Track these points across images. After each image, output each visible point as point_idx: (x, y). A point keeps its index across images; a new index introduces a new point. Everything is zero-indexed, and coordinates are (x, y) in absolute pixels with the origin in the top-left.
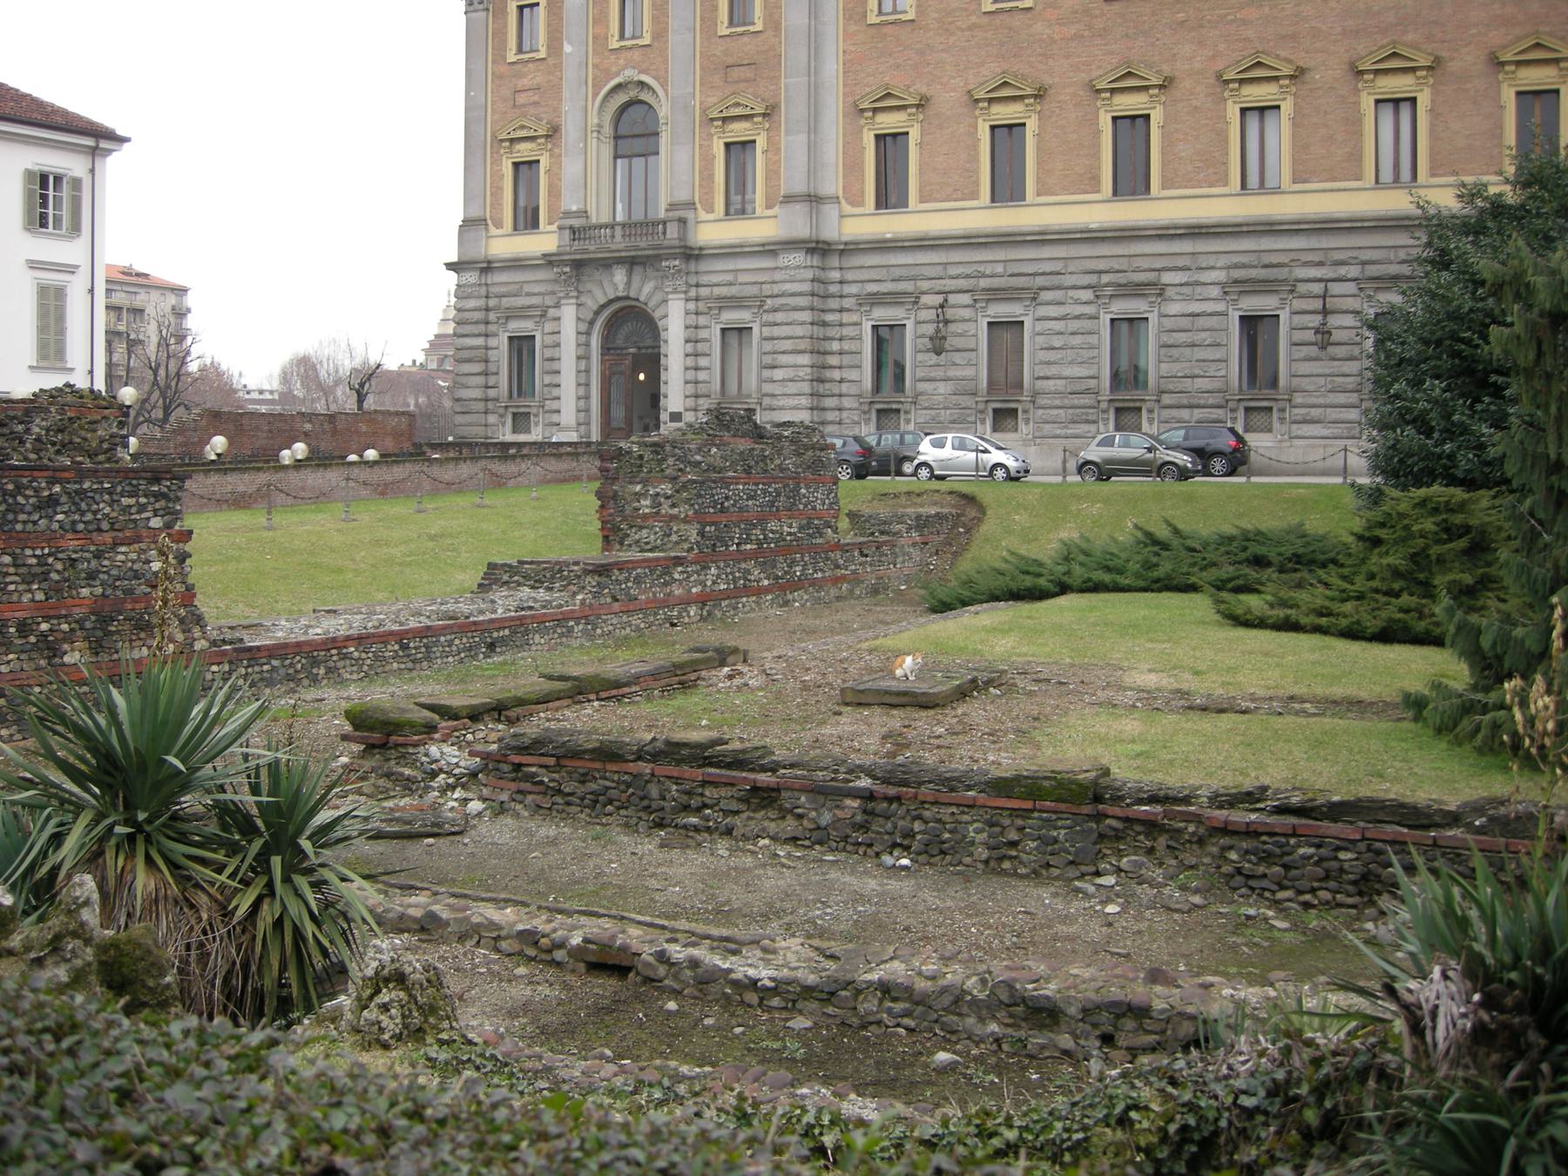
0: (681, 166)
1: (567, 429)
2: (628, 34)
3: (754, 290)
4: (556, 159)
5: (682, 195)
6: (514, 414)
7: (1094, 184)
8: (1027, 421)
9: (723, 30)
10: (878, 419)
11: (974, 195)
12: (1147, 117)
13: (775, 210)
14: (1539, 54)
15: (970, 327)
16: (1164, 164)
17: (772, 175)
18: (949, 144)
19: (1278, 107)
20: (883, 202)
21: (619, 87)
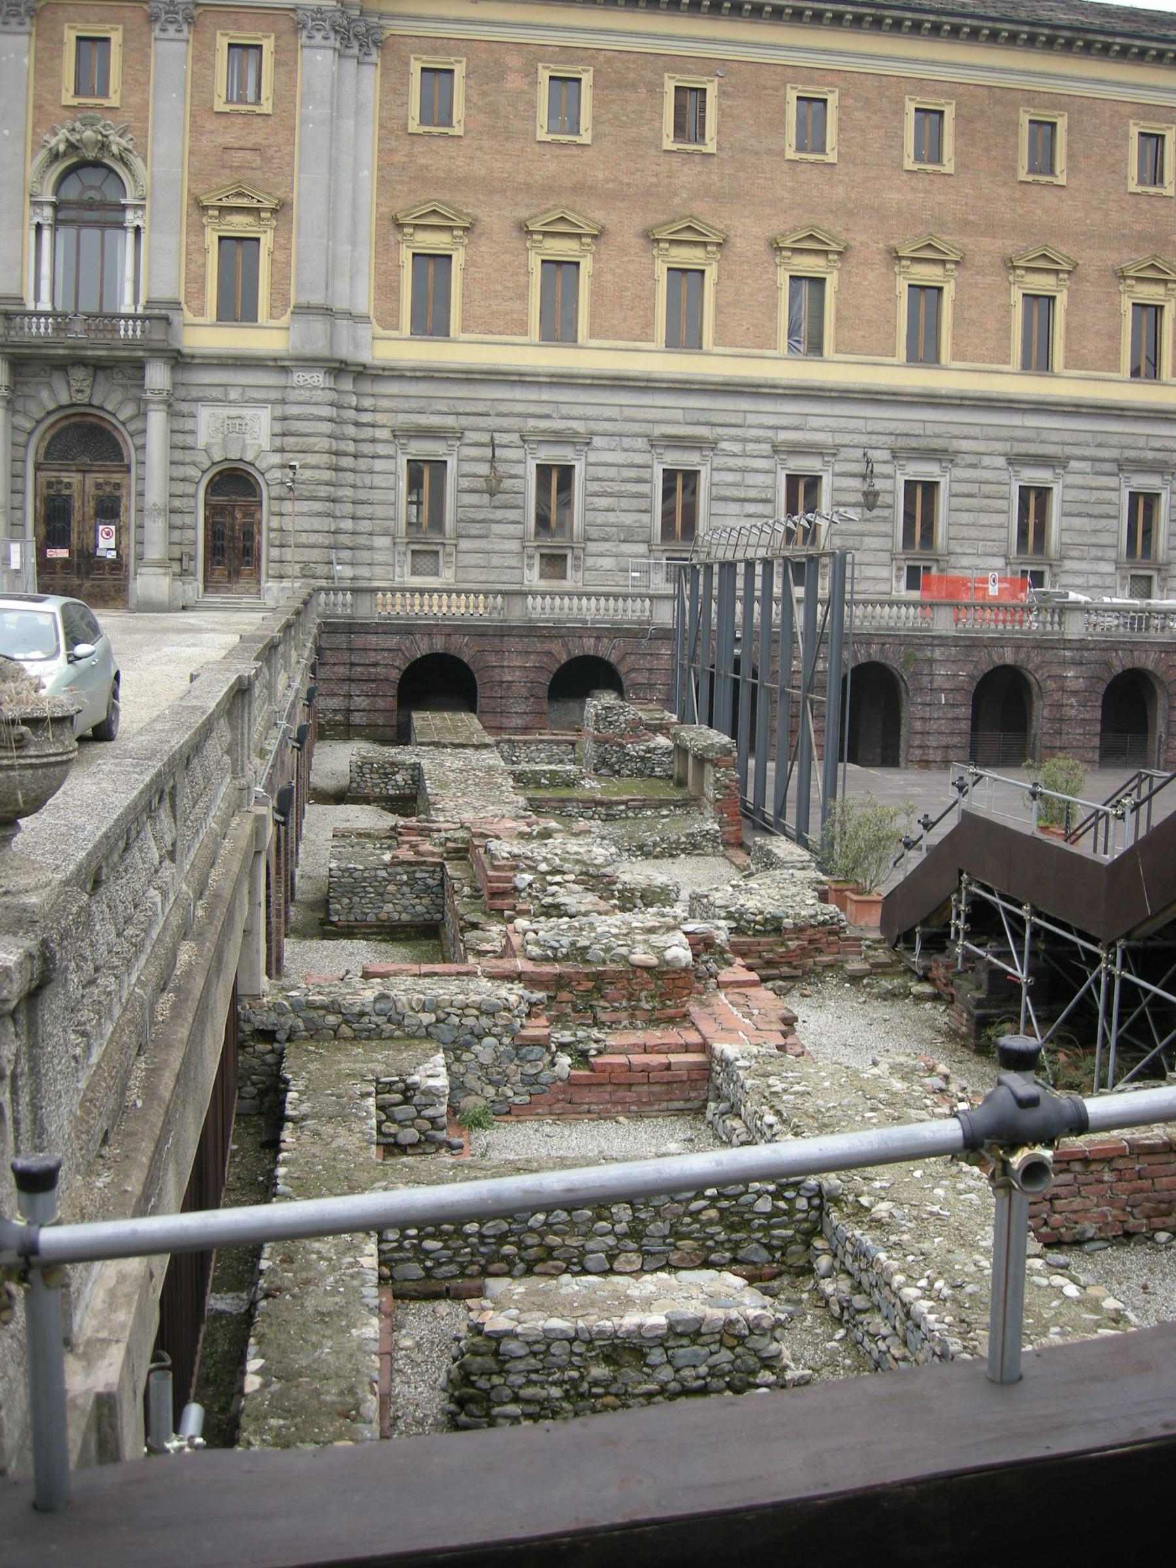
8: (576, 568)
13: (284, 320)
14: (1156, 275)
19: (258, 240)
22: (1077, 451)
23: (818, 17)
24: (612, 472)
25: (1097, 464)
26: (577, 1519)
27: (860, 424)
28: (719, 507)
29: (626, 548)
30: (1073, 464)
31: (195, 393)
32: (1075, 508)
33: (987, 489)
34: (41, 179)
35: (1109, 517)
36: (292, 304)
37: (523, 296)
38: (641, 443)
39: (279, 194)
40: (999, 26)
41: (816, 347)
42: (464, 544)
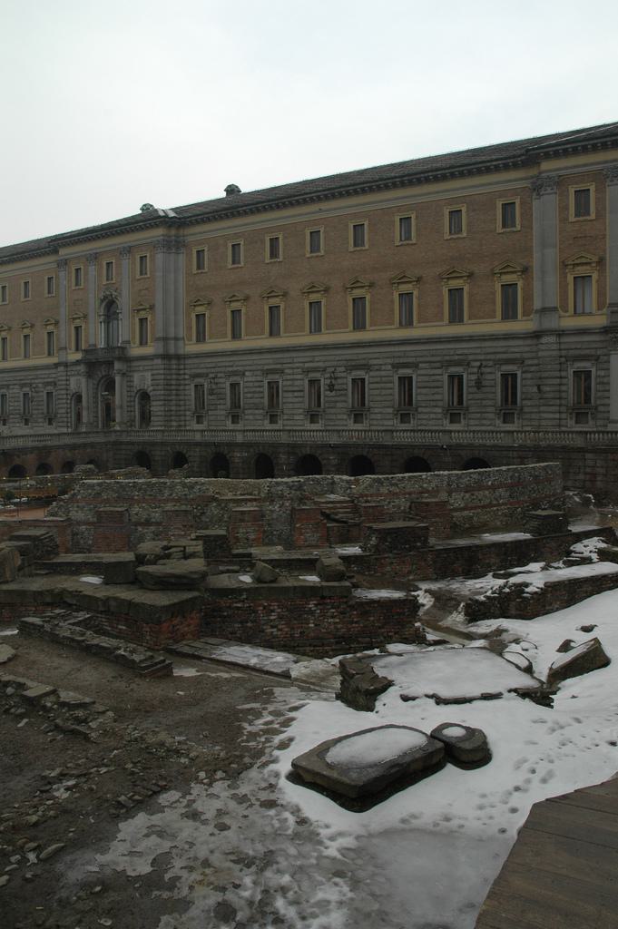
0: (126, 329)
2: (403, 239)
5: (126, 338)
7: (224, 336)
8: (593, 419)
9: (572, 218)
10: (576, 417)
11: (442, 320)
12: (204, 314)
15: (492, 377)
19: (591, 276)
20: (198, 340)
22: (421, 359)
24: (251, 384)
25: (432, 364)
26: (486, 880)
27: (332, 358)
28: (286, 395)
29: (257, 412)
34: (99, 308)
35: (438, 387)
40: (566, 146)
42: (210, 413)
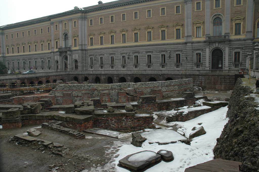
0: (70, 42)
1: (207, 67)
3: (181, 49)
4: (244, 22)
5: (70, 45)
6: (162, 65)
7: (120, 42)
8: (201, 66)
9: (214, 8)
10: (235, 66)
12: (93, 38)
16: (105, 42)
17: (244, 27)
18: (97, 38)
21: (215, 15)
22: (154, 50)
23: (137, 3)
27: (129, 50)
29: (108, 65)
30: (153, 52)
31: (73, 53)
32: (154, 57)
33: (143, 56)
36: (246, 31)
37: (99, 41)
38: (108, 54)
39: (244, 16)
41: (137, 41)
